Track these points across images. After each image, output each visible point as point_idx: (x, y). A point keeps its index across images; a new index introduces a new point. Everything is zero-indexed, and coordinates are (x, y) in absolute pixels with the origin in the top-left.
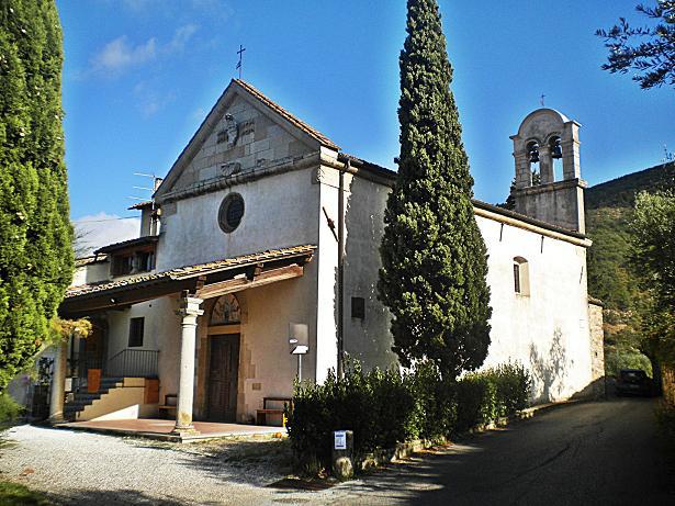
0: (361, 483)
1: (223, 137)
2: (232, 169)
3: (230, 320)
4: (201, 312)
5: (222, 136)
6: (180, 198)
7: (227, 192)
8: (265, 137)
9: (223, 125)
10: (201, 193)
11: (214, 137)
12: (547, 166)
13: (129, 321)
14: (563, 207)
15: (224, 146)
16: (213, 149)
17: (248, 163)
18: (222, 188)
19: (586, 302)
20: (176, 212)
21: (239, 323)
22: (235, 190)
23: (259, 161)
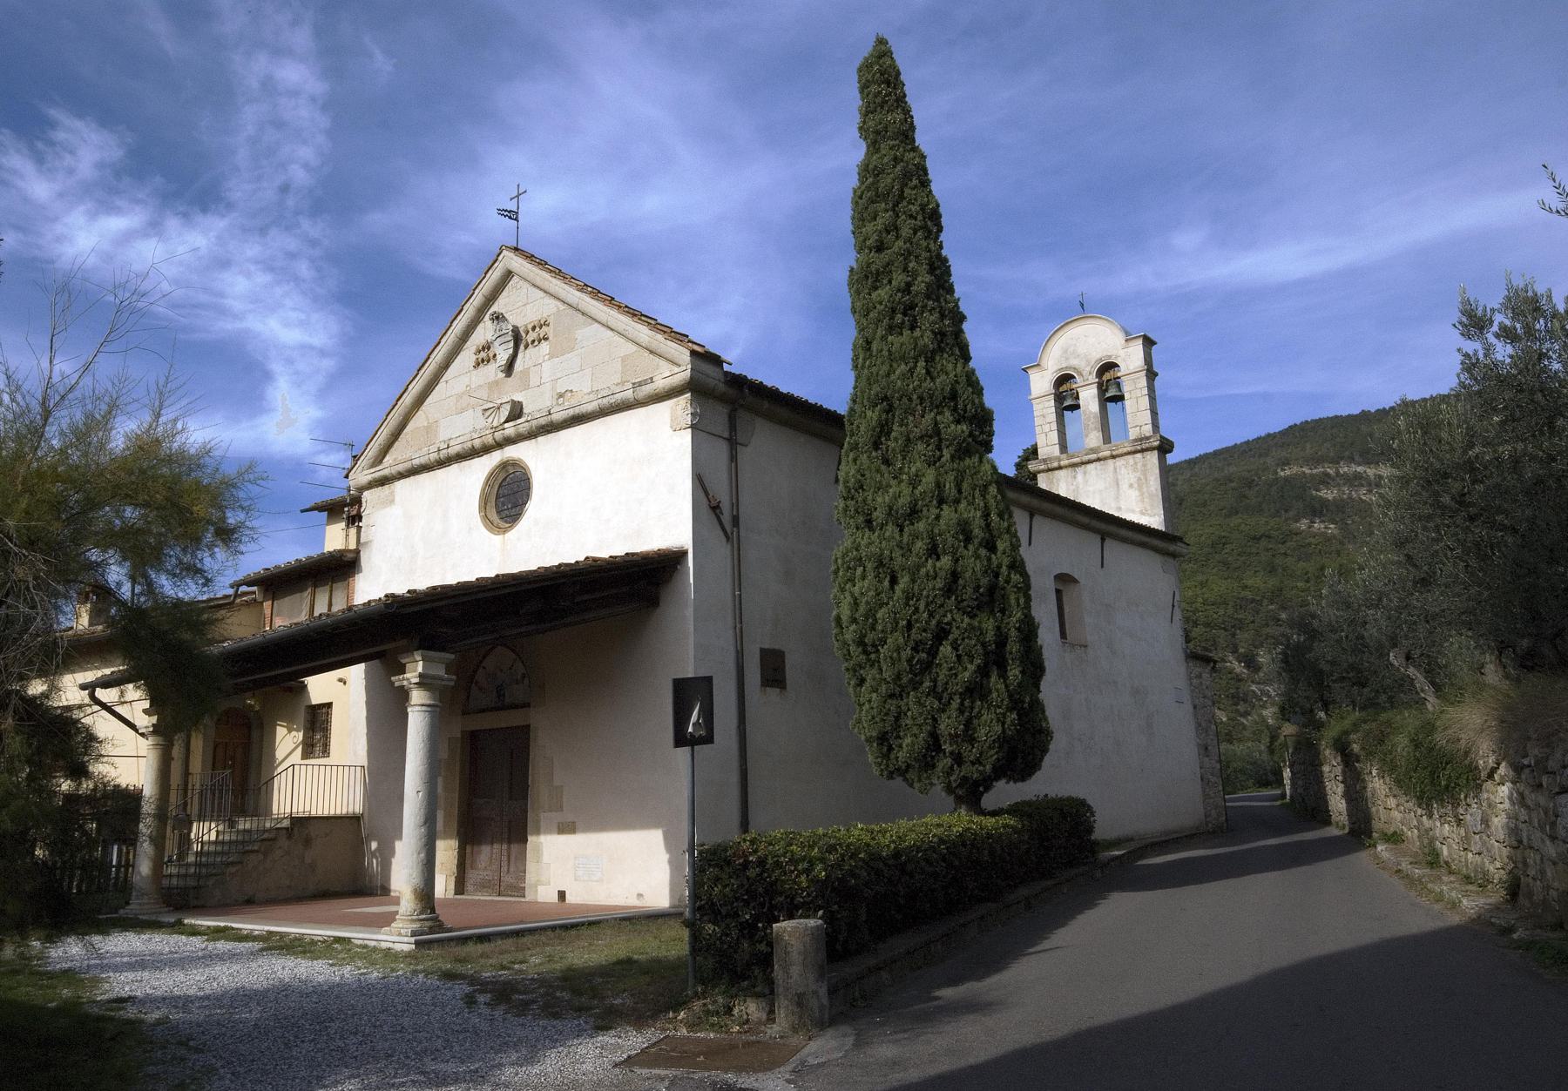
0: (196, 781)
1: (485, 356)
2: (505, 412)
3: (508, 700)
4: (154, 719)
5: (483, 355)
6: (402, 476)
7: (495, 458)
8: (572, 350)
9: (485, 331)
10: (442, 463)
11: (467, 357)
12: (734, 526)
13: (303, 708)
14: (1131, 486)
15: (493, 371)
16: (465, 380)
17: (537, 405)
18: (486, 450)
19: (1181, 656)
20: (392, 501)
21: (526, 705)
22: (511, 452)
23: (561, 396)
